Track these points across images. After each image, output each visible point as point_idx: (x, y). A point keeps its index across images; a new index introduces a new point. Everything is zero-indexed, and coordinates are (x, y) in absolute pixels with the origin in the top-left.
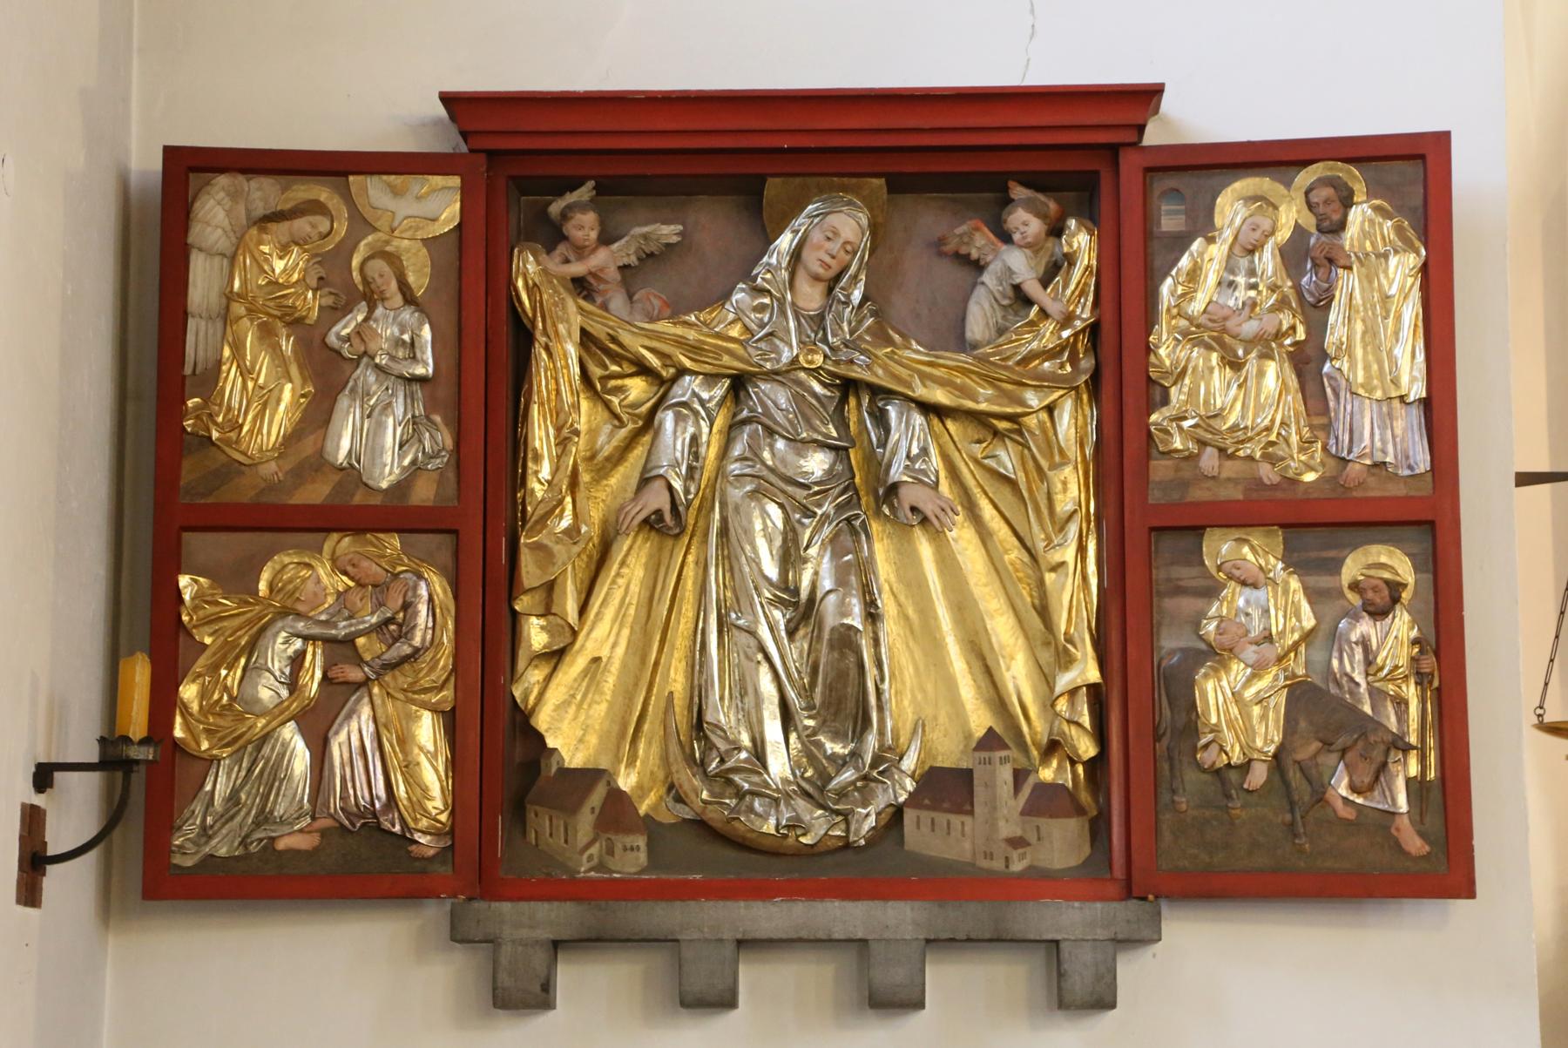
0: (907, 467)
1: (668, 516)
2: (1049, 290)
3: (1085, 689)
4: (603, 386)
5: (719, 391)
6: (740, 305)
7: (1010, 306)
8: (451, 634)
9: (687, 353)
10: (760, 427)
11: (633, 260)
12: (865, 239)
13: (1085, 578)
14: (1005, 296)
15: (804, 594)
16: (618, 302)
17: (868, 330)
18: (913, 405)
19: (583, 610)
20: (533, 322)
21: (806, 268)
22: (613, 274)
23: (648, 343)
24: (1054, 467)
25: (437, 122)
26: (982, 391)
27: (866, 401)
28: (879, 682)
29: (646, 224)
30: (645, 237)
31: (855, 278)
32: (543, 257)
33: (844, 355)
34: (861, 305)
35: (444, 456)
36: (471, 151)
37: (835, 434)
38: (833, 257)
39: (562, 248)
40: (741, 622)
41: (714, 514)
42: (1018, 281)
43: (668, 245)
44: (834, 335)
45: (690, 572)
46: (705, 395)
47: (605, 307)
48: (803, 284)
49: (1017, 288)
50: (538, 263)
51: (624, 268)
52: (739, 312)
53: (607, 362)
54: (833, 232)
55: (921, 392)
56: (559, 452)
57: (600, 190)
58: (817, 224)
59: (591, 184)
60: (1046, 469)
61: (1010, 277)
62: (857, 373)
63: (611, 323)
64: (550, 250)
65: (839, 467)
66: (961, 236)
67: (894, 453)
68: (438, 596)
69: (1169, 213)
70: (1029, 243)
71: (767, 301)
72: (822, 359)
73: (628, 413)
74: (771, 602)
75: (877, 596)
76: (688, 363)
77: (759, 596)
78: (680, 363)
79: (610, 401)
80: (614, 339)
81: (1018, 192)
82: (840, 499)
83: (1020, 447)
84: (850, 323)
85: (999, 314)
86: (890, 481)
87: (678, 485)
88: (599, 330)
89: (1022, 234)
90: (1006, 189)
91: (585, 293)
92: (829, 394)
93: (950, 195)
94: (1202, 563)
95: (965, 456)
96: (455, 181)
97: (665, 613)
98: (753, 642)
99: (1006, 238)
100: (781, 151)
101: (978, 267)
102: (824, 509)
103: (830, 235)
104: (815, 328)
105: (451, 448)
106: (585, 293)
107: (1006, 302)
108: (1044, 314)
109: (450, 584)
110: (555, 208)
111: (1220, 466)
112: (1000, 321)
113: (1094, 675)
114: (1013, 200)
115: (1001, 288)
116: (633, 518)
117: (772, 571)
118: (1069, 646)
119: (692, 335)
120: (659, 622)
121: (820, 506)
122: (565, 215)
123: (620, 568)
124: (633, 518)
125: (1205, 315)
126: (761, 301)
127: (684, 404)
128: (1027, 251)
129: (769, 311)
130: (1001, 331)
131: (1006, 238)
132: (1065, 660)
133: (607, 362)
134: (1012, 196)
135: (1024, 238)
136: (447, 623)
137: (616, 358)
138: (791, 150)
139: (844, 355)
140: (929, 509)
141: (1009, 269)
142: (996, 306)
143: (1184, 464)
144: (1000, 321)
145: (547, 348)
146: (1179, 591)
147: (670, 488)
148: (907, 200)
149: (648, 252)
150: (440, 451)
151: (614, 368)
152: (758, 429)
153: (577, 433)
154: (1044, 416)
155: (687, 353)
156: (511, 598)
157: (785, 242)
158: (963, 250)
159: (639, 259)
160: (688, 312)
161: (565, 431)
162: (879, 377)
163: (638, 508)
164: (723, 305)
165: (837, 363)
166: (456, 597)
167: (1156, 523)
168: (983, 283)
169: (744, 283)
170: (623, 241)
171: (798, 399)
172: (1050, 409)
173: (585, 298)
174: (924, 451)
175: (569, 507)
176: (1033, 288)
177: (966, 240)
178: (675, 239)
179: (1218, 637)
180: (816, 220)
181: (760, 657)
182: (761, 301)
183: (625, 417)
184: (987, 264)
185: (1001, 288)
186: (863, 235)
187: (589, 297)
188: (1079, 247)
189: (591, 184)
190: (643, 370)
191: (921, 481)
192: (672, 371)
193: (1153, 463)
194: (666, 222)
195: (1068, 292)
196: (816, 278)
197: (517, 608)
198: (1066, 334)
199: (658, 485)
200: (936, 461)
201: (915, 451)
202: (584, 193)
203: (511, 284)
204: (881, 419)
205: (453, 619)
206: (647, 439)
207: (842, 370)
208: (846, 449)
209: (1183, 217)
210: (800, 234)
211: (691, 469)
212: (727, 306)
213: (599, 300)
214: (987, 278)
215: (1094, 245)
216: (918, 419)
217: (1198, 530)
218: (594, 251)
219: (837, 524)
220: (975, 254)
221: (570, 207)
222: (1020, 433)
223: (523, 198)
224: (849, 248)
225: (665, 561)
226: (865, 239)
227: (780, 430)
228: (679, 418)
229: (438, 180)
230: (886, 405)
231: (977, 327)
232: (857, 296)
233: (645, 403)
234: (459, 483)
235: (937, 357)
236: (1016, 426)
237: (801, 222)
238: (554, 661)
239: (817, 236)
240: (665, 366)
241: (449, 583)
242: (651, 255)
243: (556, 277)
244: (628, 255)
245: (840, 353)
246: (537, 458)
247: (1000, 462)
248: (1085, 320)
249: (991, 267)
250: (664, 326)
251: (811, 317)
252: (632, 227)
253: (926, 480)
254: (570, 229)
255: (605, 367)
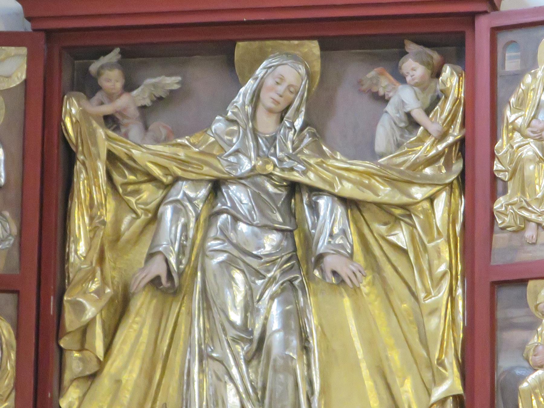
0: (329, 242)
1: (164, 280)
2: (431, 116)
3: (451, 398)
4: (124, 190)
5: (203, 192)
6: (218, 132)
7: (406, 127)
8: (13, 363)
9: (180, 166)
10: (229, 217)
11: (147, 102)
12: (303, 83)
13: (453, 320)
14: (401, 121)
15: (257, 334)
16: (135, 131)
17: (307, 147)
18: (336, 199)
19: (108, 348)
20: (77, 147)
21: (263, 105)
22: (133, 112)
23: (152, 158)
24: (431, 240)
25: (17, 14)
26: (382, 187)
27: (305, 199)
28: (309, 396)
29: (154, 77)
30: (155, 85)
31: (298, 110)
32: (84, 101)
33: (287, 163)
34: (302, 129)
35: (10, 240)
36: (34, 30)
37: (280, 220)
38: (281, 96)
39: (99, 96)
40: (214, 355)
41: (197, 279)
42: (408, 109)
43: (171, 91)
44: (281, 150)
45: (183, 320)
46: (192, 195)
47: (126, 136)
48: (261, 114)
49: (409, 115)
50: (79, 105)
51: (143, 108)
52: (216, 137)
53: (126, 173)
54: (281, 79)
55: (337, 190)
56: (92, 235)
57: (125, 54)
58: (270, 74)
59: (117, 50)
60: (426, 242)
61: (403, 107)
62: (296, 177)
63: (129, 146)
64: (90, 96)
65: (285, 243)
66: (371, 79)
67: (321, 233)
68: (4, 336)
69: (511, 58)
70: (417, 83)
71: (235, 128)
72: (272, 167)
73: (142, 209)
74: (234, 340)
75: (309, 334)
76: (179, 173)
77: (226, 335)
78: (174, 173)
79: (129, 200)
80: (131, 158)
81: (412, 47)
82: (285, 266)
83: (411, 228)
84: (293, 142)
85: (398, 134)
86: (318, 253)
87: (173, 260)
88: (119, 150)
89: (412, 76)
90: (402, 46)
91: (115, 126)
92: (279, 192)
93: (369, 51)
94: (527, 306)
95: (375, 235)
96: (24, 50)
97: (165, 349)
98: (221, 368)
99: (402, 79)
100: (242, 23)
101: (384, 100)
102: (272, 273)
103: (278, 80)
104: (269, 146)
105: (16, 234)
106: (115, 126)
107: (402, 125)
108: (427, 133)
109: (12, 326)
110: (94, 67)
111: (537, 236)
112: (399, 138)
113: (459, 389)
114: (407, 53)
115: (398, 115)
116: (140, 282)
117: (236, 317)
118: (441, 368)
119: (182, 154)
120: (161, 355)
121: (269, 271)
122: (99, 73)
123: (135, 318)
124: (140, 282)
125: (529, 129)
126: (232, 128)
127: (178, 201)
128: (416, 88)
129: (238, 134)
130: (399, 145)
131: (402, 79)
132: (438, 379)
133: (126, 173)
134: (407, 50)
135: (413, 80)
136: (10, 355)
137: (133, 170)
138: (248, 23)
139: (287, 163)
140: (345, 271)
141: (403, 102)
142: (395, 127)
143: (514, 236)
144: (399, 138)
145: (84, 164)
146: (513, 326)
147: (167, 261)
148: (337, 55)
149: (157, 96)
150: (8, 236)
151: (132, 178)
152: (228, 218)
153: (104, 223)
154: (426, 205)
155: (180, 166)
156: (58, 338)
157: (250, 85)
158: (375, 89)
159: (152, 101)
160: (180, 136)
161: (96, 221)
162: (311, 179)
163: (144, 275)
164: (206, 131)
165: (283, 170)
166: (17, 337)
167: (496, 279)
168: (386, 112)
169: (221, 116)
170: (140, 89)
171: (256, 197)
172: (431, 199)
173: (114, 130)
174: (344, 232)
175: (98, 273)
176: (419, 115)
177: (375, 82)
178: (176, 87)
179: (534, 357)
180: (269, 71)
181: (227, 378)
182: (232, 128)
183: (139, 212)
184: (390, 98)
185: (398, 115)
186: (302, 80)
187: (117, 129)
188: (451, 86)
189: (117, 50)
190: (152, 179)
191: (339, 253)
192: (170, 178)
193: (495, 236)
194: (170, 75)
195: (443, 117)
196: (270, 111)
197: (62, 345)
198: (440, 147)
199: (158, 259)
200: (354, 237)
201: (336, 231)
202: (114, 56)
203: (61, 121)
204: (314, 208)
205: (15, 352)
206: (153, 228)
207: (286, 175)
208: (291, 231)
209: (519, 60)
210: (258, 81)
211: (182, 247)
212: (209, 132)
213: (123, 130)
214: (390, 108)
215: (463, 84)
216: (340, 210)
217: (523, 282)
218: (120, 95)
219: (282, 284)
220: (381, 92)
221: (102, 67)
222: (410, 217)
223: (76, 62)
224: (292, 89)
225: (166, 312)
226: (303, 83)
227: (242, 218)
228: (176, 212)
229: (12, 50)
230: (317, 199)
231: (380, 144)
232: (298, 123)
233: (455, 293)
234: (20, 259)
235: (352, 164)
236: (408, 213)
237: (260, 72)
238: (89, 383)
239: (270, 82)
240: (166, 175)
241: (12, 326)
242: (160, 99)
243: (218, 156)
244: (144, 99)
245: (284, 163)
246: (77, 241)
247: (398, 239)
248: (455, 136)
249: (391, 101)
250: (159, 148)
251: (266, 138)
252: (145, 78)
253: (342, 251)
254: (103, 82)
255: (125, 176)
